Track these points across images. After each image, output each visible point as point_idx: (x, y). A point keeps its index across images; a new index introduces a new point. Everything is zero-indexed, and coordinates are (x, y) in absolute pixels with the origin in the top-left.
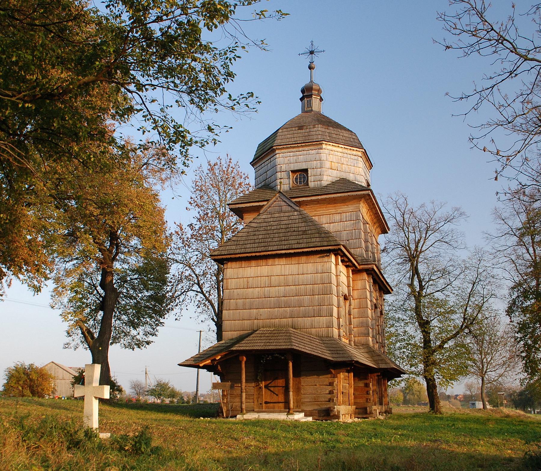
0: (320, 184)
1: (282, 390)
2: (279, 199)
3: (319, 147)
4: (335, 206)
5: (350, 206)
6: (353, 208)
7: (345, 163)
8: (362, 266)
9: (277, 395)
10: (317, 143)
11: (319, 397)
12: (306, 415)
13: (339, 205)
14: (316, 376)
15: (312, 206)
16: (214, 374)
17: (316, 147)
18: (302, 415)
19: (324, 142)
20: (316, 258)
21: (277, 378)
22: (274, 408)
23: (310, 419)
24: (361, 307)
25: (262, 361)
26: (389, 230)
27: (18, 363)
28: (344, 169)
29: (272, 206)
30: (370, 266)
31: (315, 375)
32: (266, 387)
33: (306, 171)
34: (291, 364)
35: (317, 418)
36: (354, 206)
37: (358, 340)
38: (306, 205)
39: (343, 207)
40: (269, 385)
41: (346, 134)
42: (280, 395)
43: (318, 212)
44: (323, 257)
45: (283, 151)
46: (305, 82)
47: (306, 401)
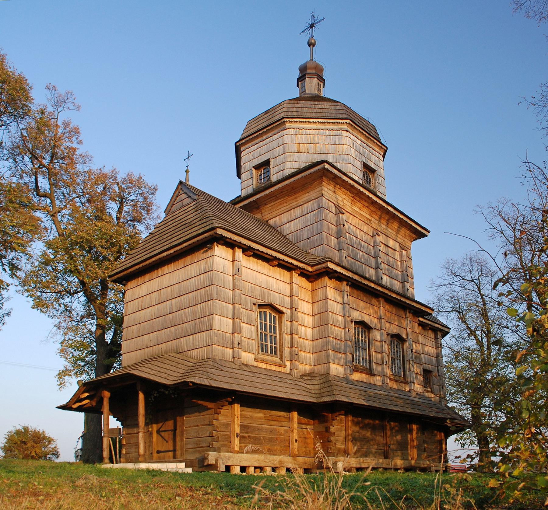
0: (283, 174)
1: (171, 433)
2: (182, 192)
3: (282, 128)
4: (296, 198)
5: (311, 193)
6: (315, 195)
7: (320, 142)
8: (315, 268)
9: (167, 442)
10: (278, 123)
11: (200, 441)
12: (187, 466)
13: (299, 194)
14: (197, 414)
15: (273, 204)
16: (117, 420)
17: (280, 129)
18: (183, 465)
19: (285, 120)
20: (199, 255)
21: (167, 420)
22: (164, 458)
23: (190, 470)
24: (322, 324)
25: (150, 399)
26: (429, 232)
27: (29, 427)
28: (318, 150)
29: (175, 203)
30: (324, 265)
31: (196, 412)
32: (158, 432)
33: (267, 163)
34: (141, 396)
35: (196, 469)
36: (316, 190)
37: (318, 369)
38: (265, 204)
39: (304, 196)
40: (161, 430)
41: (325, 105)
42: (169, 442)
43: (279, 211)
44: (206, 251)
45: (247, 146)
46: (304, 59)
47: (189, 447)
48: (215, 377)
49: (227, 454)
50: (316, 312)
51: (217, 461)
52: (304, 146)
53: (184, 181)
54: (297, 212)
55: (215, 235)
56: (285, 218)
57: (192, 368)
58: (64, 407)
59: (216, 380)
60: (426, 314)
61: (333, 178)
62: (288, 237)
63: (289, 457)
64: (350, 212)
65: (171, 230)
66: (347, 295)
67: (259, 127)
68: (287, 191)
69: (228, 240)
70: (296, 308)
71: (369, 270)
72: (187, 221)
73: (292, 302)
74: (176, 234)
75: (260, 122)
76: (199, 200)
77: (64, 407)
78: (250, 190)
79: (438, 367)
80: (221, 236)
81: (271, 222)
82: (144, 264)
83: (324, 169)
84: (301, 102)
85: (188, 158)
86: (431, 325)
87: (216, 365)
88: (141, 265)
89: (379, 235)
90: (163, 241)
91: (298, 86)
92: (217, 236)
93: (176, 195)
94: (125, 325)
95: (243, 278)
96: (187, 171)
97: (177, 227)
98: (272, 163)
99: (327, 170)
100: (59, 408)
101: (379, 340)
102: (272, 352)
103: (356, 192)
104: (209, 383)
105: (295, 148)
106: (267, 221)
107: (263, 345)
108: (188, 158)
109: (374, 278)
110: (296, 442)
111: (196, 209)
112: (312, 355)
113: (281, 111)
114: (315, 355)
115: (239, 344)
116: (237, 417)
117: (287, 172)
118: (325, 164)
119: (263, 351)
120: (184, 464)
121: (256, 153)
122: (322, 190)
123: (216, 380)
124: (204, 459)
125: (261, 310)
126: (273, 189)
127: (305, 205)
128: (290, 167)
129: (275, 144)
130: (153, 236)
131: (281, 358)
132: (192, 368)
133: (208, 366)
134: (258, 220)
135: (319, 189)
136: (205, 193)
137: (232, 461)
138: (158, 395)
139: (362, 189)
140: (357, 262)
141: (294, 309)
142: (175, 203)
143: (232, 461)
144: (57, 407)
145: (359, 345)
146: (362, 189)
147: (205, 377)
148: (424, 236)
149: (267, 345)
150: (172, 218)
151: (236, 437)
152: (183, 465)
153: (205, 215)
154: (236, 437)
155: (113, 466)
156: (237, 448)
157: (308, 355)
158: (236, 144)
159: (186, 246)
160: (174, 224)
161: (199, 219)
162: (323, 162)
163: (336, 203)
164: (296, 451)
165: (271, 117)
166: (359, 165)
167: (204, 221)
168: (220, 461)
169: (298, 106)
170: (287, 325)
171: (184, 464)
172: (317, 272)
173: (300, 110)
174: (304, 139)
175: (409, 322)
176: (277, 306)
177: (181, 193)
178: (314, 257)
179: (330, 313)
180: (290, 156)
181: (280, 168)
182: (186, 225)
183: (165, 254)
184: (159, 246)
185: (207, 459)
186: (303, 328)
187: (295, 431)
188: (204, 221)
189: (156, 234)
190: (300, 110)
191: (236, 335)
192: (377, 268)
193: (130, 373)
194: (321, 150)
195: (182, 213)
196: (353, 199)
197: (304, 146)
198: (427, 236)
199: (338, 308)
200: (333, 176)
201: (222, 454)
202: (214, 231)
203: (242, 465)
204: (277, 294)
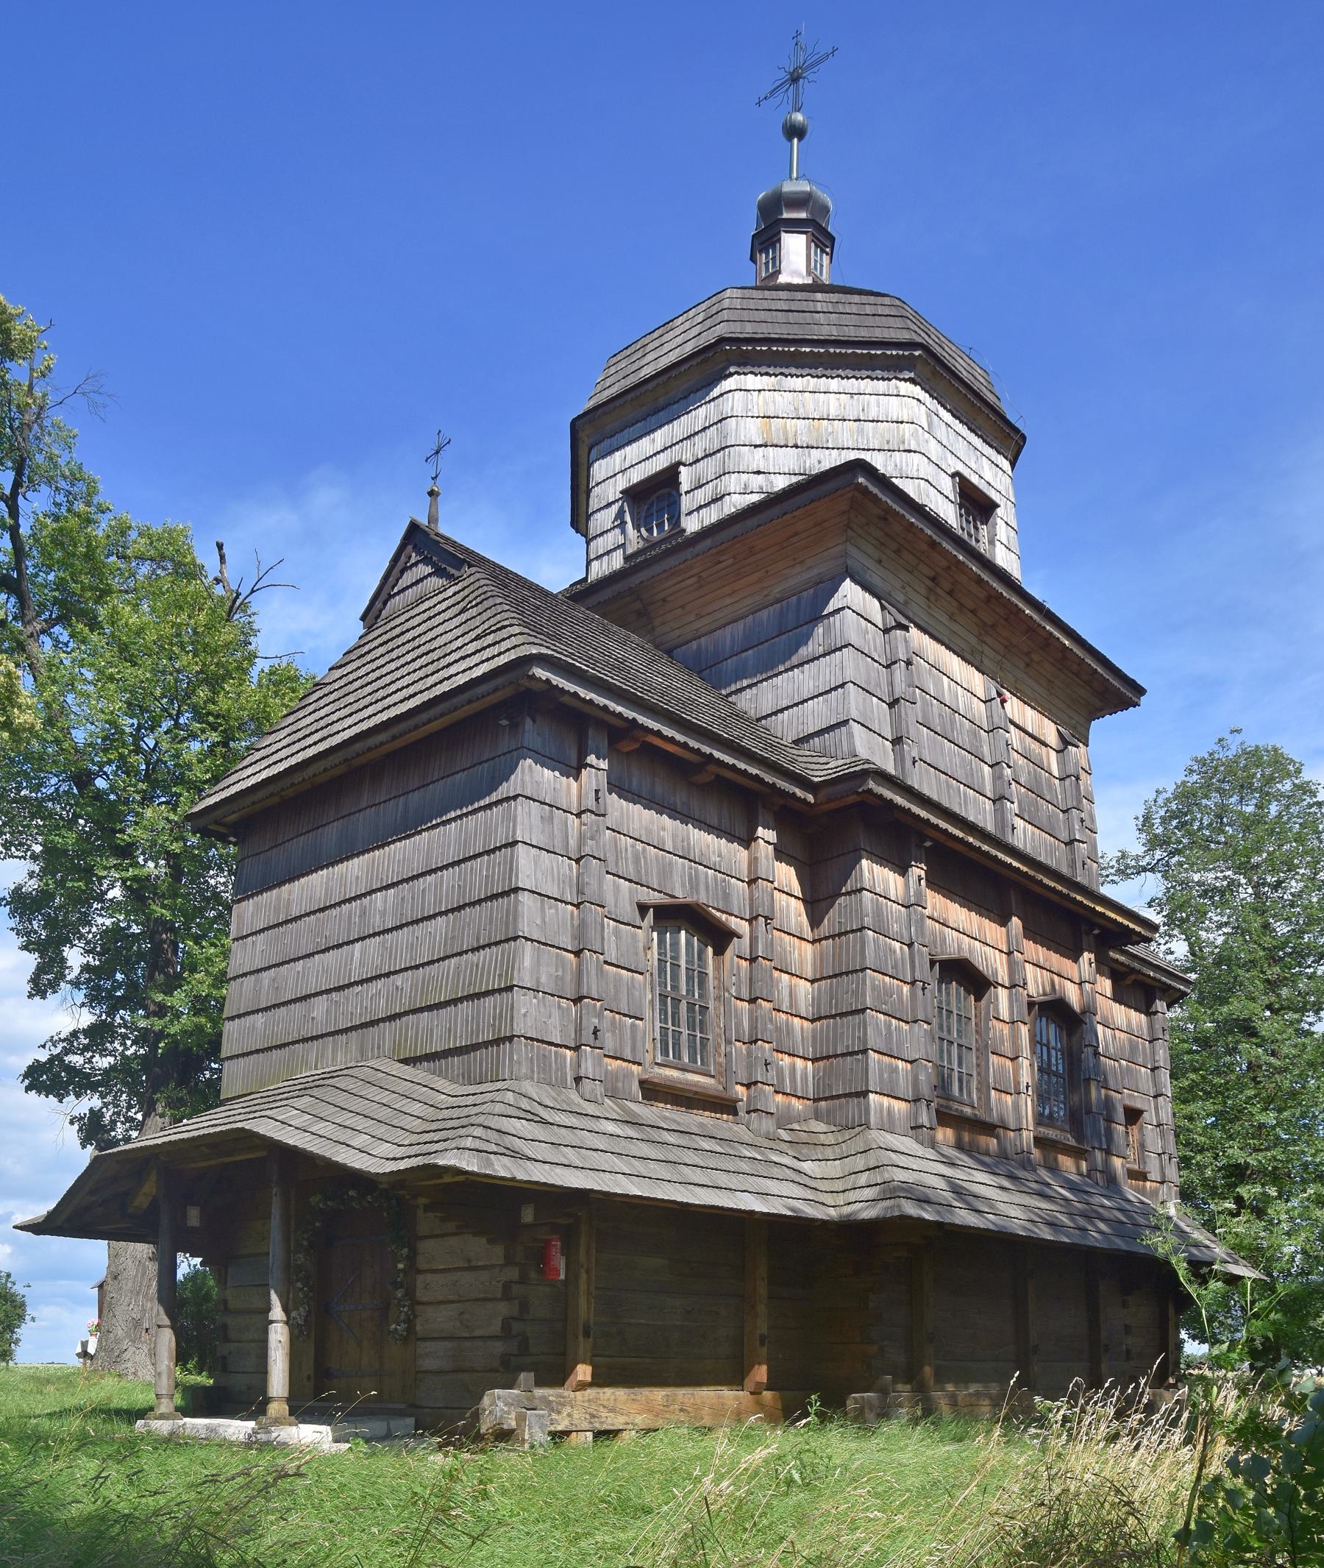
29: (395, 590)
48: (528, 1149)
53: (423, 520)
57: (446, 1114)
58: (37, 1228)
59: (529, 1159)
60: (1135, 938)
61: (879, 517)
65: (384, 671)
68: (734, 558)
69: (565, 699)
71: (644, 850)
74: (399, 684)
77: (37, 1228)
80: (546, 687)
85: (437, 452)
87: (525, 1104)
91: (753, 259)
92: (533, 685)
93: (397, 566)
97: (402, 661)
99: (865, 491)
101: (1007, 1018)
103: (944, 563)
107: (667, 1035)
108: (437, 452)
109: (990, 827)
110: (762, 1344)
111: (462, 605)
112: (810, 1063)
123: (529, 1159)
132: (446, 1114)
133: (499, 1108)
136: (488, 561)
137: (569, 1415)
142: (395, 590)
143: (569, 1415)
144: (14, 1227)
145: (675, 987)
147: (494, 1148)
148: (1126, 704)
150: (385, 638)
154: (581, 1338)
157: (799, 1063)
160: (394, 655)
161: (473, 635)
166: (947, 485)
167: (490, 639)
172: (833, 806)
177: (413, 560)
186: (785, 977)
187: (762, 1309)
188: (490, 639)
192: (998, 799)
198: (1135, 705)
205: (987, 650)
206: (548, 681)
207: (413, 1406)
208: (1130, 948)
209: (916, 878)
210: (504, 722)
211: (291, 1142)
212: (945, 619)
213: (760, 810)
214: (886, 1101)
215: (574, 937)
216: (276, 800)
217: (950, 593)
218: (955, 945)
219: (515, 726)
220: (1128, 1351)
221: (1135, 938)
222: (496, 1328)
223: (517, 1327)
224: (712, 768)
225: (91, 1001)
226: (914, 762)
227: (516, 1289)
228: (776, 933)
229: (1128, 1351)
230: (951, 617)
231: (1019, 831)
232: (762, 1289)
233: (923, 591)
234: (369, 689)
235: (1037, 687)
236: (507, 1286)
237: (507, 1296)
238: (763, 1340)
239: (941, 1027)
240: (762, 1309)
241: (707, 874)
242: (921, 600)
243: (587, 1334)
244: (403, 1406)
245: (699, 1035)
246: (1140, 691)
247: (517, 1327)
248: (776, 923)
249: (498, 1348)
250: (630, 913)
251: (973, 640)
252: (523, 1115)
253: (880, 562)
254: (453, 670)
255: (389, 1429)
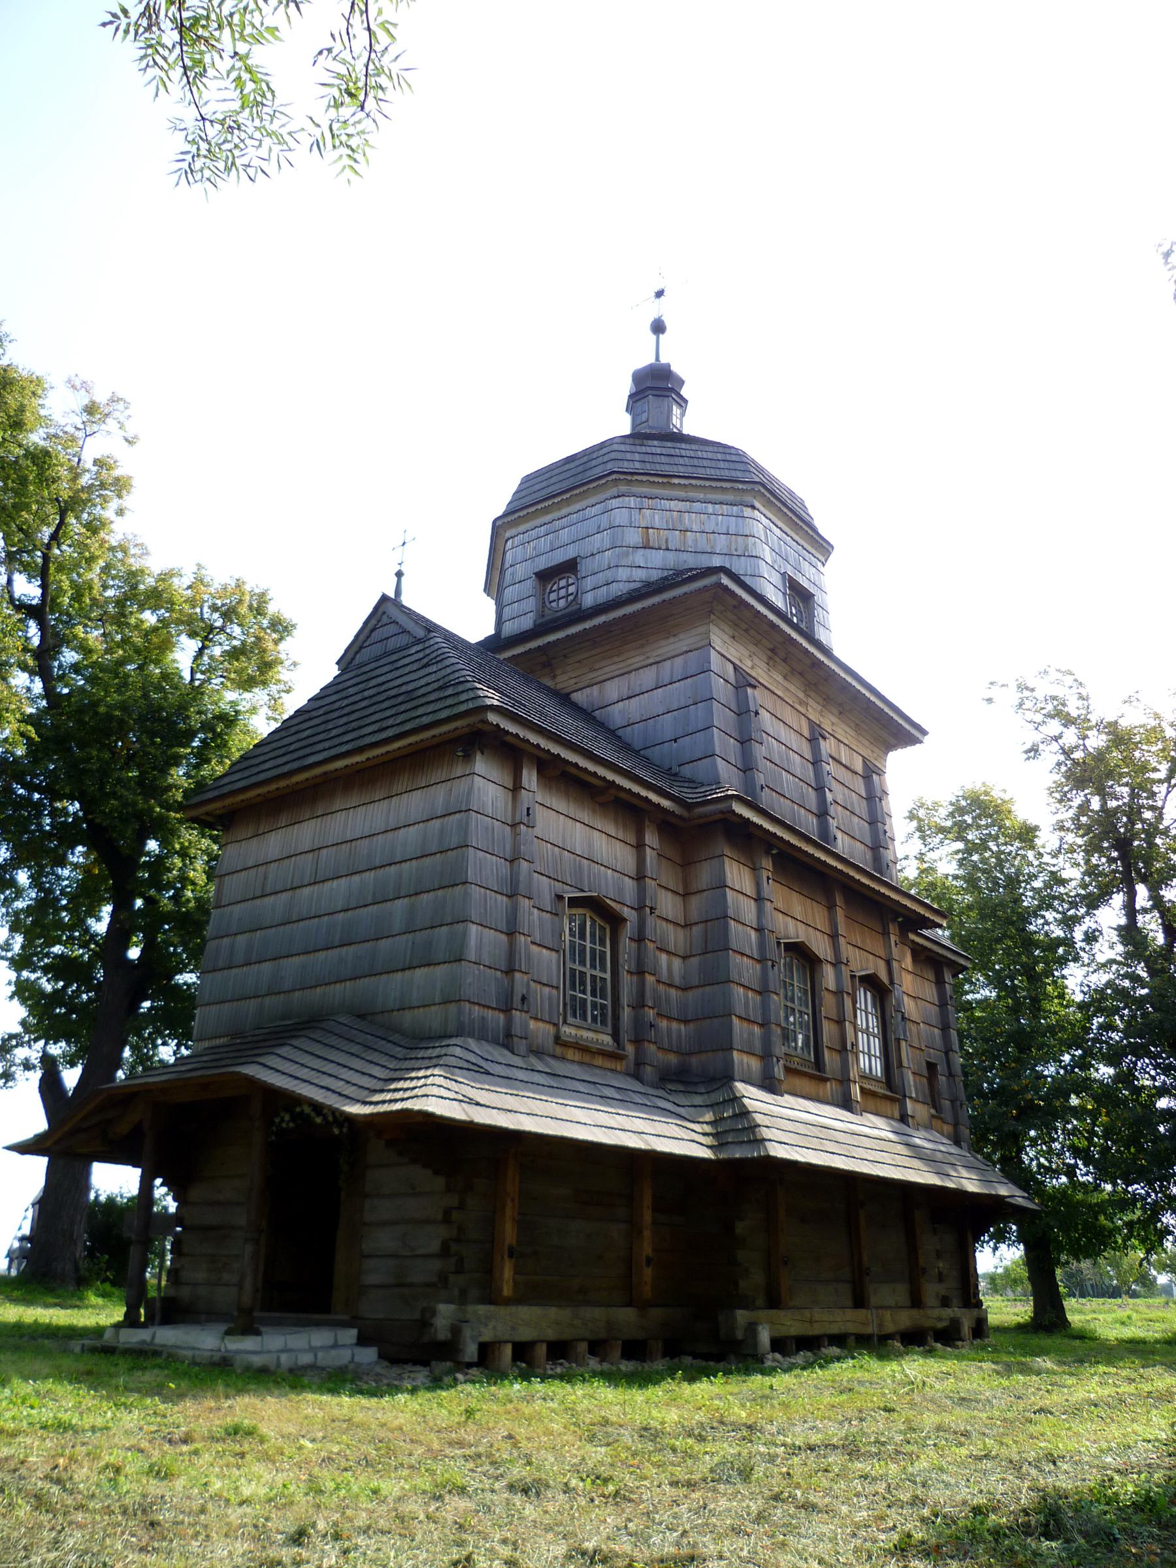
4: (642, 646)
7: (695, 528)
18: (349, 1335)
38: (565, 656)
46: (645, 359)
49: (482, 1309)
50: (694, 916)
51: (456, 1331)
52: (659, 534)
53: (392, 595)
54: (647, 677)
55: (480, 726)
56: (613, 690)
62: (620, 733)
63: (629, 1309)
64: (766, 684)
66: (768, 878)
67: (550, 490)
69: (508, 738)
70: (651, 908)
72: (404, 689)
73: (641, 892)
75: (554, 480)
76: (432, 642)
78: (527, 623)
79: (946, 1053)
81: (577, 697)
82: (282, 784)
83: (719, 585)
84: (650, 442)
86: (930, 950)
87: (473, 1059)
88: (273, 787)
89: (824, 738)
90: (334, 733)
92: (486, 728)
94: (209, 931)
95: (538, 831)
96: (399, 574)
98: (584, 567)
99: (726, 588)
100: (10, 1148)
102: (594, 1018)
104: (467, 1114)
105: (633, 537)
106: (569, 694)
113: (606, 458)
114: (691, 1026)
115: (524, 999)
116: (513, 1200)
117: (618, 589)
118: (722, 576)
119: (586, 1020)
120: (354, 1332)
121: (543, 543)
122: (708, 633)
123: (478, 1104)
124: (425, 1323)
125: (574, 911)
126: (587, 625)
127: (668, 664)
128: (626, 579)
129: (590, 526)
130: (306, 716)
131: (616, 1036)
134: (548, 689)
135: (702, 629)
138: (291, 1125)
139: (794, 635)
140: (782, 799)
141: (648, 910)
146: (794, 635)
148: (913, 741)
149: (585, 1000)
151: (506, 1257)
152: (349, 1335)
153: (452, 677)
154: (506, 1257)
155: (153, 1338)
156: (507, 1291)
157: (674, 1025)
158: (494, 522)
159: (399, 748)
162: (722, 569)
163: (738, 662)
164: (647, 1292)
165: (580, 469)
168: (467, 1333)
169: (644, 449)
170: (627, 946)
171: (354, 1332)
173: (648, 458)
174: (658, 519)
175: (893, 944)
176: (608, 901)
178: (692, 785)
179: (732, 922)
180: (627, 554)
181: (601, 578)
182: (400, 699)
183: (340, 764)
184: (327, 744)
185: (431, 1325)
187: (647, 1234)
189: (315, 714)
190: (648, 458)
191: (517, 975)
193: (239, 1073)
194: (696, 545)
195: (386, 669)
196: (770, 654)
197: (659, 534)
198: (921, 742)
199: (748, 910)
200: (735, 603)
201: (470, 1308)
202: (480, 717)
203: (518, 1339)
204: (610, 871)
205: (811, 702)
206: (498, 725)
207: (355, 1318)
208: (925, 932)
209: (765, 879)
210: (460, 754)
211: (279, 1084)
212: (780, 678)
213: (647, 823)
214: (745, 1058)
215: (508, 922)
216: (260, 799)
217: (785, 660)
218: (794, 931)
219: (468, 757)
220: (940, 1274)
221: (929, 924)
222: (435, 1246)
223: (454, 1248)
224: (613, 791)
225: (1162, 1179)
226: (762, 788)
227: (455, 1215)
228: (659, 922)
229: (940, 1274)
230: (785, 677)
231: (839, 841)
232: (648, 1216)
233: (765, 658)
234: (345, 720)
235: (848, 730)
236: (447, 1213)
237: (447, 1219)
238: (649, 1261)
239: (786, 997)
240: (647, 1234)
241: (606, 874)
242: (763, 665)
243: (511, 1256)
244: (346, 1317)
245: (589, 998)
246: (924, 732)
247: (454, 1248)
248: (657, 912)
249: (437, 1265)
250: (547, 902)
251: (801, 695)
252: (472, 1067)
253: (733, 637)
254: (420, 711)
255: (336, 1340)
